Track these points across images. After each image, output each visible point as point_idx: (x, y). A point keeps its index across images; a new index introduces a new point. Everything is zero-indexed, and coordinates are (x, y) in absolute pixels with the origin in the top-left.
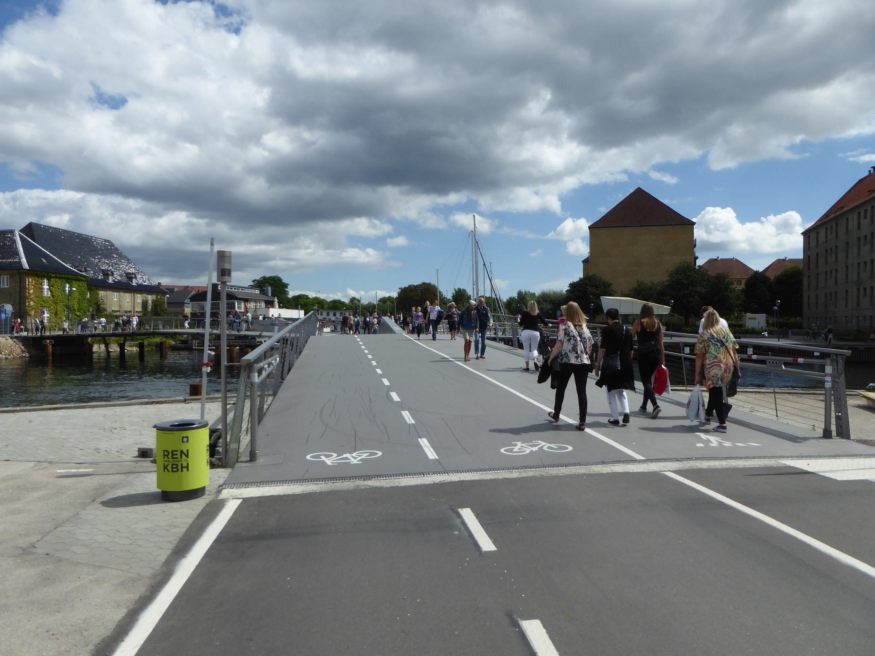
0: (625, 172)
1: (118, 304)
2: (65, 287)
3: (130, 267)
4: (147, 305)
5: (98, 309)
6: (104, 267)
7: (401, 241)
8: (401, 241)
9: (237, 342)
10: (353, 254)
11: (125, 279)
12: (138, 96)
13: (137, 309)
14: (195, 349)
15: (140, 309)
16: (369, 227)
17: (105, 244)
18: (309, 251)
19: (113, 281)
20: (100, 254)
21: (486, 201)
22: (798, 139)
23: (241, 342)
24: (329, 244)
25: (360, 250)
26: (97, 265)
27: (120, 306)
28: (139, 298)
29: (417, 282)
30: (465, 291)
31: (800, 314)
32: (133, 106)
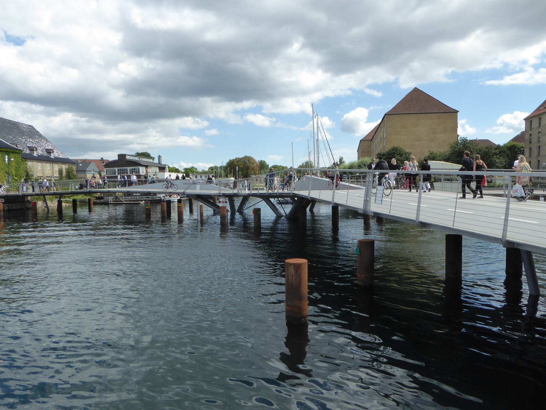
0: (350, 89)
1: (42, 171)
2: (4, 158)
3: (48, 145)
4: (62, 172)
5: (28, 175)
6: (30, 145)
7: (214, 132)
8: (214, 132)
9: (142, 198)
10: (184, 140)
11: (46, 154)
12: (33, 38)
13: (55, 175)
14: (111, 204)
15: (57, 175)
16: (193, 123)
17: (29, 128)
18: (156, 138)
19: (37, 154)
20: (27, 135)
21: (267, 106)
22: (450, 70)
23: (139, 198)
24: (168, 133)
25: (189, 137)
26: (24, 143)
27: (43, 173)
28: (56, 167)
29: (241, 156)
30: (265, 162)
32: (30, 44)
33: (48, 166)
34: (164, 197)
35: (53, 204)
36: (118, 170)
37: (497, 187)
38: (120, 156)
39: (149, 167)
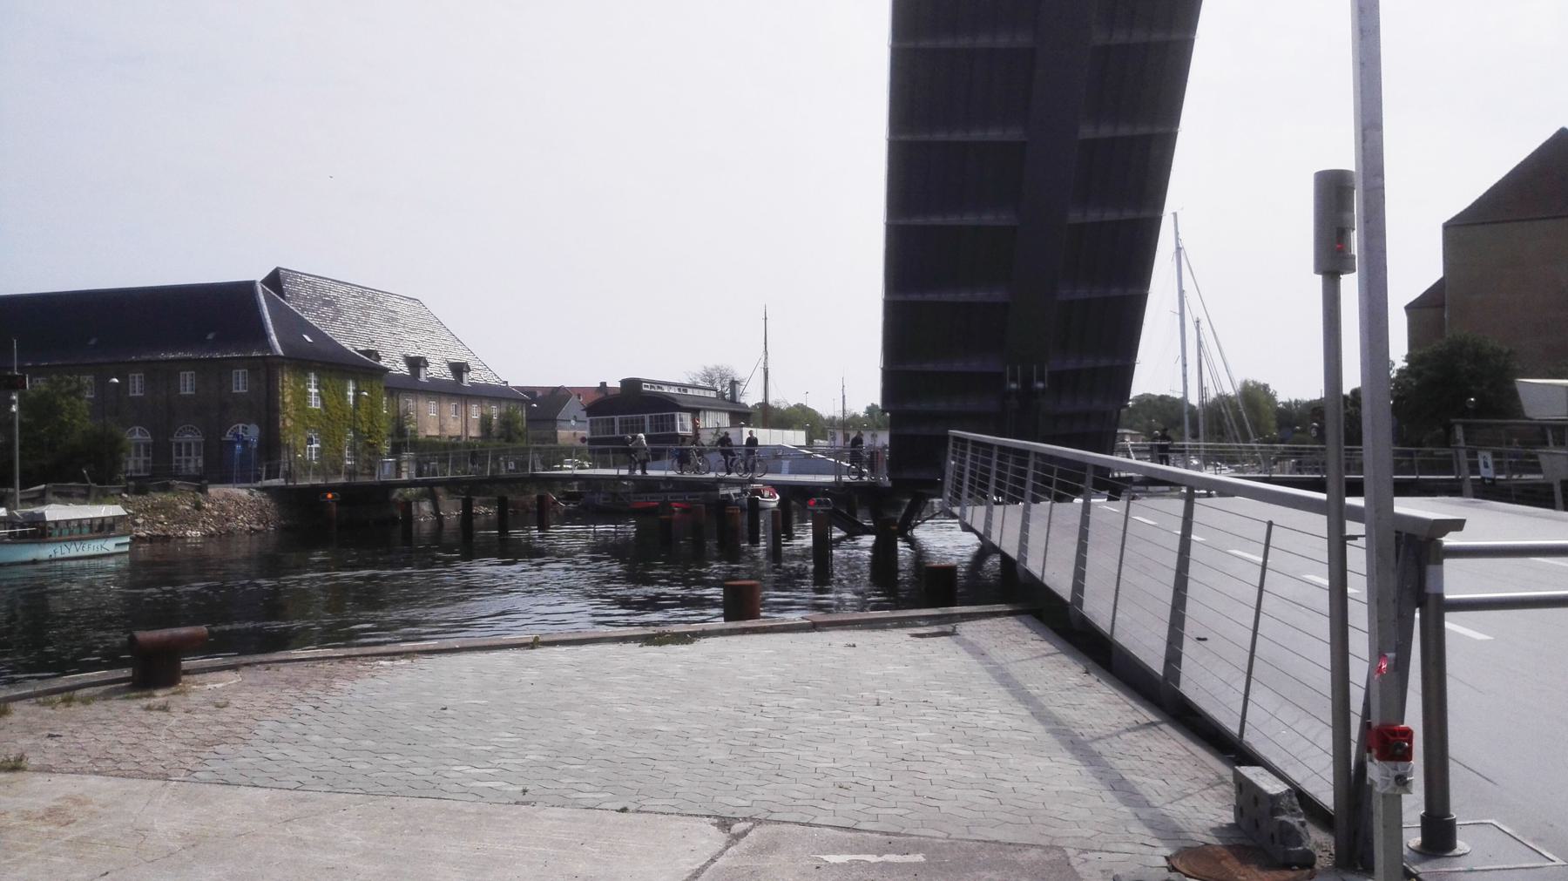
4: (490, 424)
23: (689, 497)
28: (475, 412)
31: (1361, 444)
33: (450, 408)
34: (738, 495)
35: (452, 511)
36: (621, 422)
37: (633, 812)
38: (601, 383)
39: (701, 413)
